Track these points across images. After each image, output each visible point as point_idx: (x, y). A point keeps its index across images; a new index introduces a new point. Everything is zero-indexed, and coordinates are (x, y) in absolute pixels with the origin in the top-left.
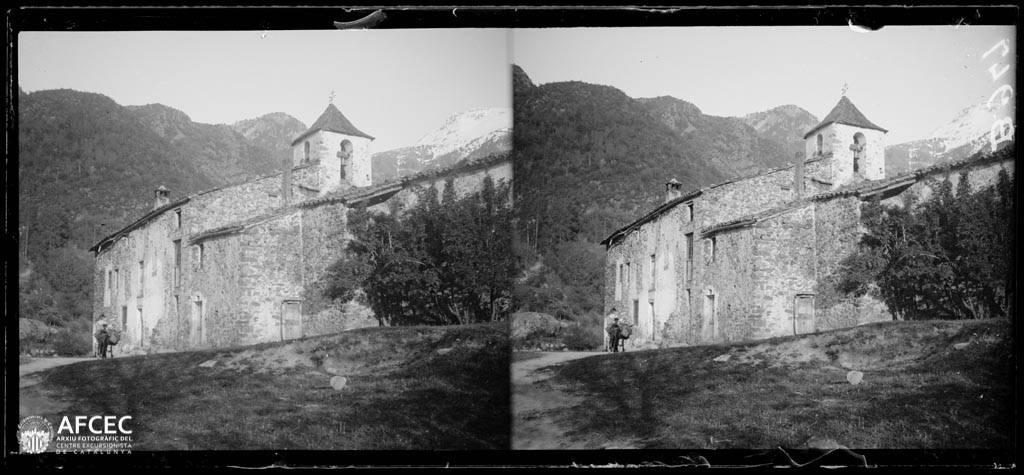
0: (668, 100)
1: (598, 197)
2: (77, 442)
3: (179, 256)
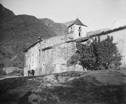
0: (46, 19)
3: (40, 53)
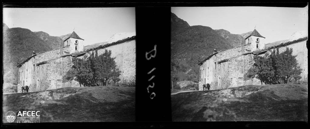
0: (41, 32)
1: (205, 53)
2: (23, 119)
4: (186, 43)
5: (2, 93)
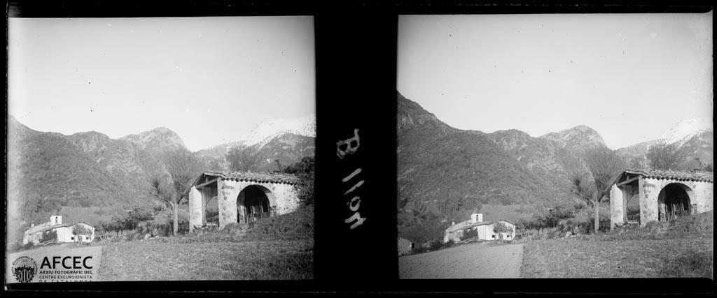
0: (93, 133)
4: (439, 169)
5: (644, 278)
